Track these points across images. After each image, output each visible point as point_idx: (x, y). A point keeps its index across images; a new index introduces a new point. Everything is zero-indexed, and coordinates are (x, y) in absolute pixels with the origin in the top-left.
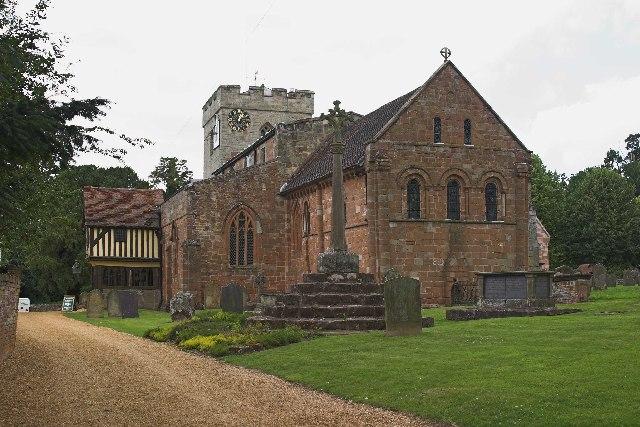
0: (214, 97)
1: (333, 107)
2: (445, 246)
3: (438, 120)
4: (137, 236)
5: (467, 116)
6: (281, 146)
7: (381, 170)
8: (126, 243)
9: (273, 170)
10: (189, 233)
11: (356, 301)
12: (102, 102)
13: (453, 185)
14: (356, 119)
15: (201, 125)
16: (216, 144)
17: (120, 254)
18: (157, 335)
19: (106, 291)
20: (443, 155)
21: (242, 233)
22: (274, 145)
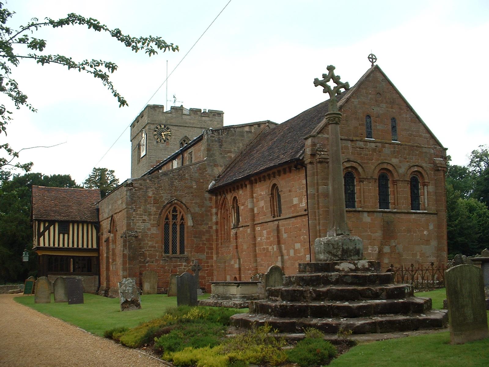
0: (141, 115)
2: (379, 234)
6: (209, 150)
7: (320, 162)
9: (202, 169)
10: (128, 225)
11: (376, 296)
14: (272, 127)
15: (130, 140)
16: (143, 154)
17: (88, 246)
18: (124, 338)
19: (53, 278)
20: (374, 150)
21: (175, 224)
22: (202, 148)
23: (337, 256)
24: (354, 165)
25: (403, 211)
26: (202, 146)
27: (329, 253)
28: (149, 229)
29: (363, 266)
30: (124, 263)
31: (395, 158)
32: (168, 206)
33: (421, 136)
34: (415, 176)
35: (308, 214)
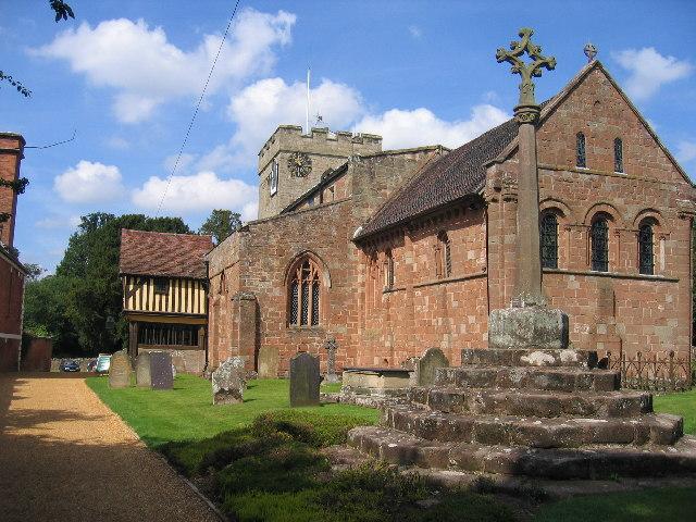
3: (581, 136)
4: (193, 293)
6: (355, 183)
7: (508, 200)
8: (167, 295)
10: (242, 283)
11: (591, 412)
12: (72, 15)
13: (600, 221)
17: (154, 309)
20: (588, 184)
22: (347, 182)
23: (526, 340)
24: (558, 205)
25: (628, 274)
26: (347, 179)
27: (513, 334)
28: (270, 290)
29: (570, 358)
30: (234, 335)
33: (657, 166)
35: (487, 275)
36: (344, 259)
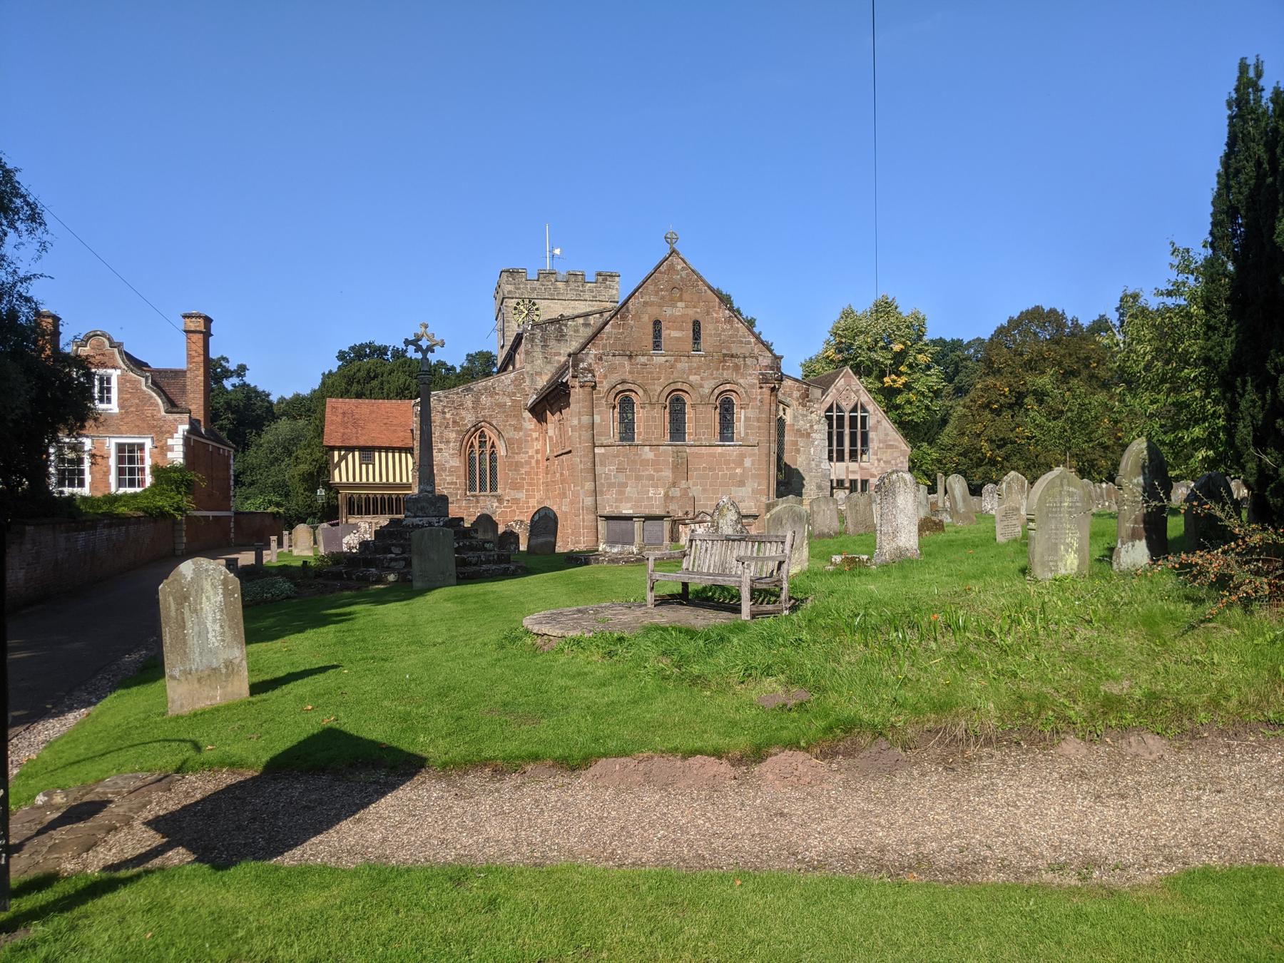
1: (437, 339)
2: (667, 474)
5: (698, 317)
8: (374, 465)
17: (401, 480)
31: (695, 374)
32: (473, 429)
34: (720, 398)
36: (518, 428)
